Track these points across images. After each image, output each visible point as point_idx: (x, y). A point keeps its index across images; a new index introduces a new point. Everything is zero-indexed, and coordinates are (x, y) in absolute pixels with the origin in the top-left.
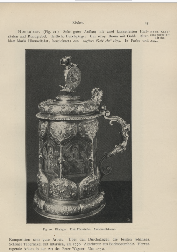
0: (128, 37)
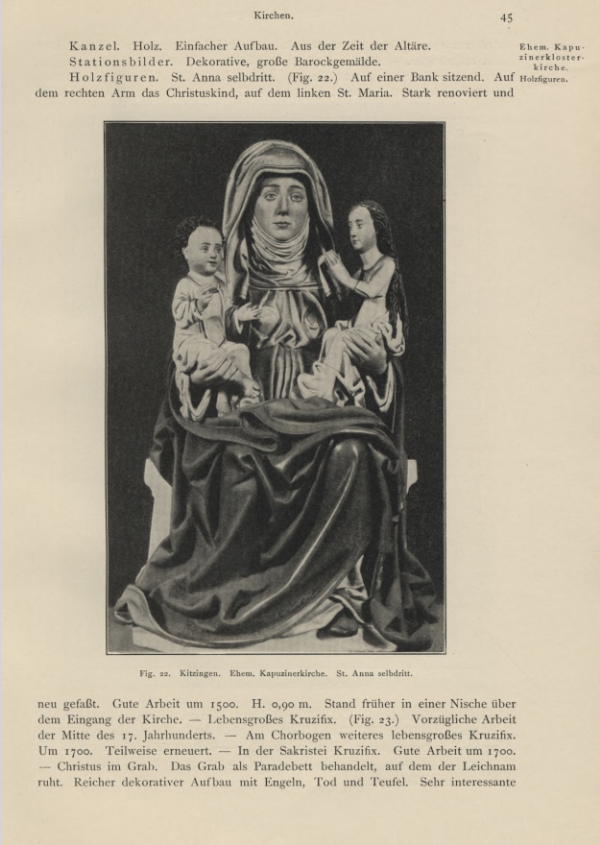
0: (398, 753)
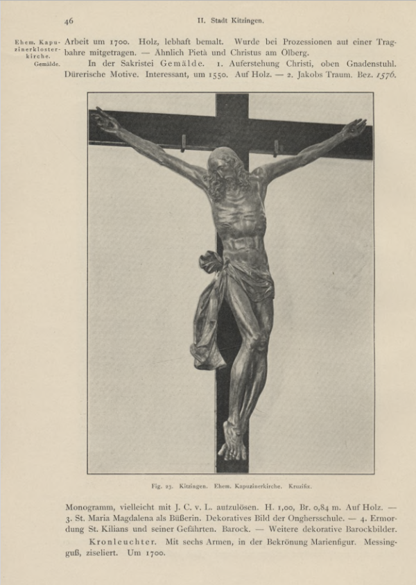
0: (180, 530)
